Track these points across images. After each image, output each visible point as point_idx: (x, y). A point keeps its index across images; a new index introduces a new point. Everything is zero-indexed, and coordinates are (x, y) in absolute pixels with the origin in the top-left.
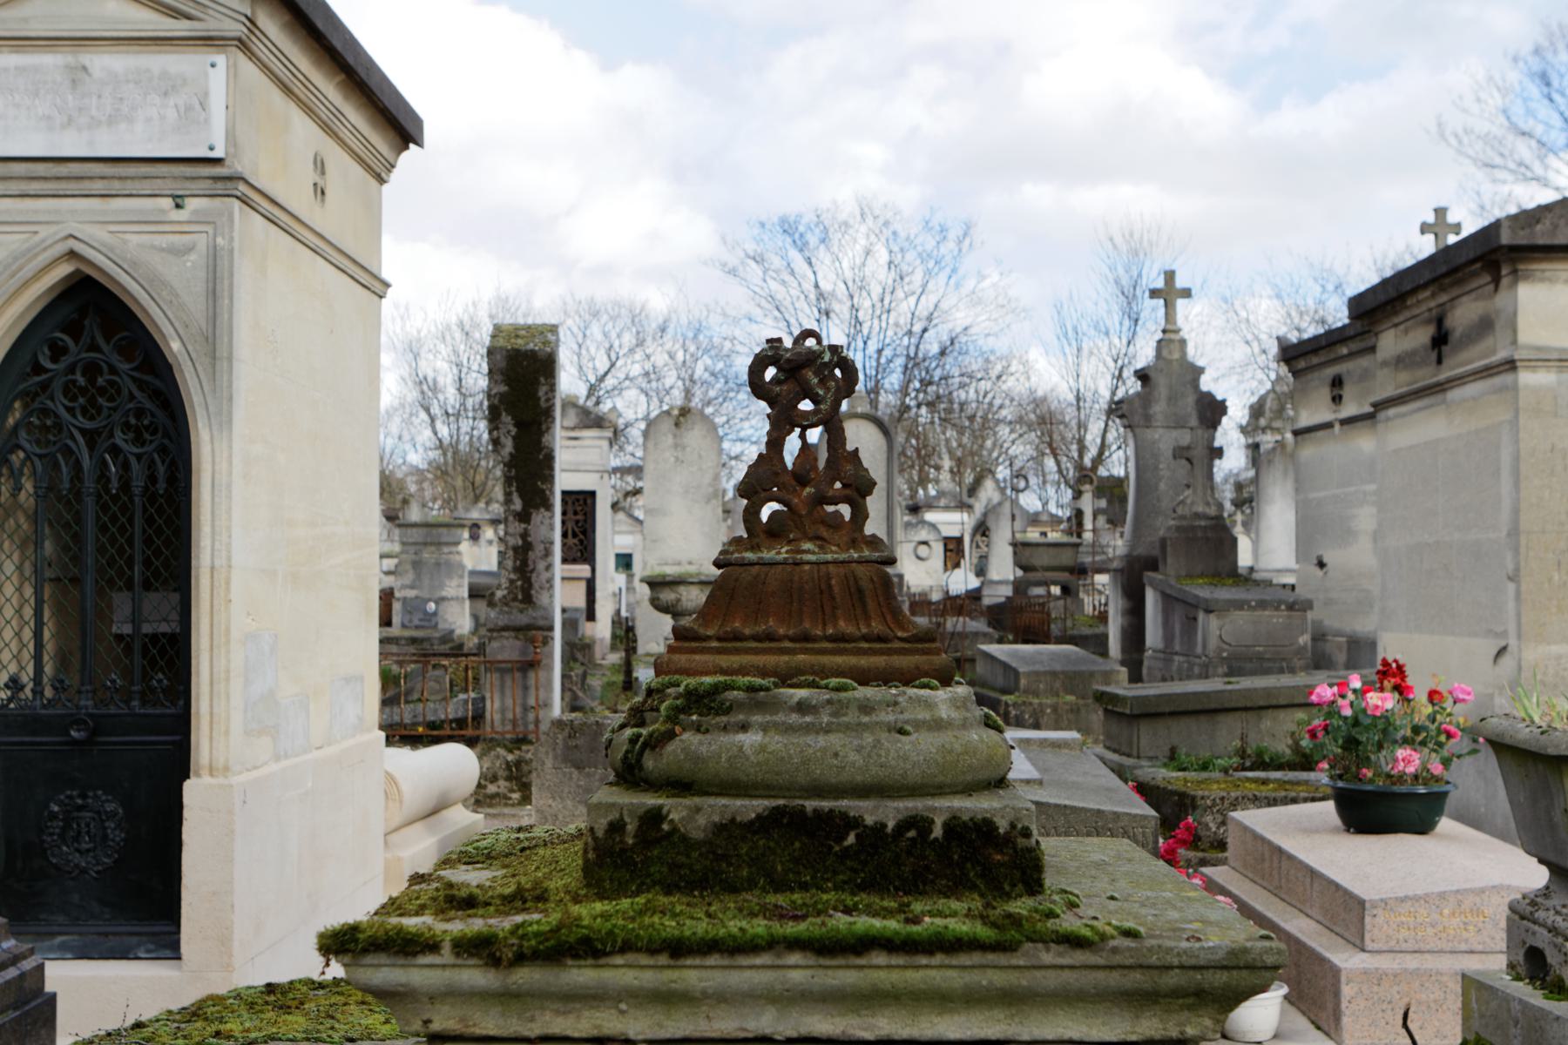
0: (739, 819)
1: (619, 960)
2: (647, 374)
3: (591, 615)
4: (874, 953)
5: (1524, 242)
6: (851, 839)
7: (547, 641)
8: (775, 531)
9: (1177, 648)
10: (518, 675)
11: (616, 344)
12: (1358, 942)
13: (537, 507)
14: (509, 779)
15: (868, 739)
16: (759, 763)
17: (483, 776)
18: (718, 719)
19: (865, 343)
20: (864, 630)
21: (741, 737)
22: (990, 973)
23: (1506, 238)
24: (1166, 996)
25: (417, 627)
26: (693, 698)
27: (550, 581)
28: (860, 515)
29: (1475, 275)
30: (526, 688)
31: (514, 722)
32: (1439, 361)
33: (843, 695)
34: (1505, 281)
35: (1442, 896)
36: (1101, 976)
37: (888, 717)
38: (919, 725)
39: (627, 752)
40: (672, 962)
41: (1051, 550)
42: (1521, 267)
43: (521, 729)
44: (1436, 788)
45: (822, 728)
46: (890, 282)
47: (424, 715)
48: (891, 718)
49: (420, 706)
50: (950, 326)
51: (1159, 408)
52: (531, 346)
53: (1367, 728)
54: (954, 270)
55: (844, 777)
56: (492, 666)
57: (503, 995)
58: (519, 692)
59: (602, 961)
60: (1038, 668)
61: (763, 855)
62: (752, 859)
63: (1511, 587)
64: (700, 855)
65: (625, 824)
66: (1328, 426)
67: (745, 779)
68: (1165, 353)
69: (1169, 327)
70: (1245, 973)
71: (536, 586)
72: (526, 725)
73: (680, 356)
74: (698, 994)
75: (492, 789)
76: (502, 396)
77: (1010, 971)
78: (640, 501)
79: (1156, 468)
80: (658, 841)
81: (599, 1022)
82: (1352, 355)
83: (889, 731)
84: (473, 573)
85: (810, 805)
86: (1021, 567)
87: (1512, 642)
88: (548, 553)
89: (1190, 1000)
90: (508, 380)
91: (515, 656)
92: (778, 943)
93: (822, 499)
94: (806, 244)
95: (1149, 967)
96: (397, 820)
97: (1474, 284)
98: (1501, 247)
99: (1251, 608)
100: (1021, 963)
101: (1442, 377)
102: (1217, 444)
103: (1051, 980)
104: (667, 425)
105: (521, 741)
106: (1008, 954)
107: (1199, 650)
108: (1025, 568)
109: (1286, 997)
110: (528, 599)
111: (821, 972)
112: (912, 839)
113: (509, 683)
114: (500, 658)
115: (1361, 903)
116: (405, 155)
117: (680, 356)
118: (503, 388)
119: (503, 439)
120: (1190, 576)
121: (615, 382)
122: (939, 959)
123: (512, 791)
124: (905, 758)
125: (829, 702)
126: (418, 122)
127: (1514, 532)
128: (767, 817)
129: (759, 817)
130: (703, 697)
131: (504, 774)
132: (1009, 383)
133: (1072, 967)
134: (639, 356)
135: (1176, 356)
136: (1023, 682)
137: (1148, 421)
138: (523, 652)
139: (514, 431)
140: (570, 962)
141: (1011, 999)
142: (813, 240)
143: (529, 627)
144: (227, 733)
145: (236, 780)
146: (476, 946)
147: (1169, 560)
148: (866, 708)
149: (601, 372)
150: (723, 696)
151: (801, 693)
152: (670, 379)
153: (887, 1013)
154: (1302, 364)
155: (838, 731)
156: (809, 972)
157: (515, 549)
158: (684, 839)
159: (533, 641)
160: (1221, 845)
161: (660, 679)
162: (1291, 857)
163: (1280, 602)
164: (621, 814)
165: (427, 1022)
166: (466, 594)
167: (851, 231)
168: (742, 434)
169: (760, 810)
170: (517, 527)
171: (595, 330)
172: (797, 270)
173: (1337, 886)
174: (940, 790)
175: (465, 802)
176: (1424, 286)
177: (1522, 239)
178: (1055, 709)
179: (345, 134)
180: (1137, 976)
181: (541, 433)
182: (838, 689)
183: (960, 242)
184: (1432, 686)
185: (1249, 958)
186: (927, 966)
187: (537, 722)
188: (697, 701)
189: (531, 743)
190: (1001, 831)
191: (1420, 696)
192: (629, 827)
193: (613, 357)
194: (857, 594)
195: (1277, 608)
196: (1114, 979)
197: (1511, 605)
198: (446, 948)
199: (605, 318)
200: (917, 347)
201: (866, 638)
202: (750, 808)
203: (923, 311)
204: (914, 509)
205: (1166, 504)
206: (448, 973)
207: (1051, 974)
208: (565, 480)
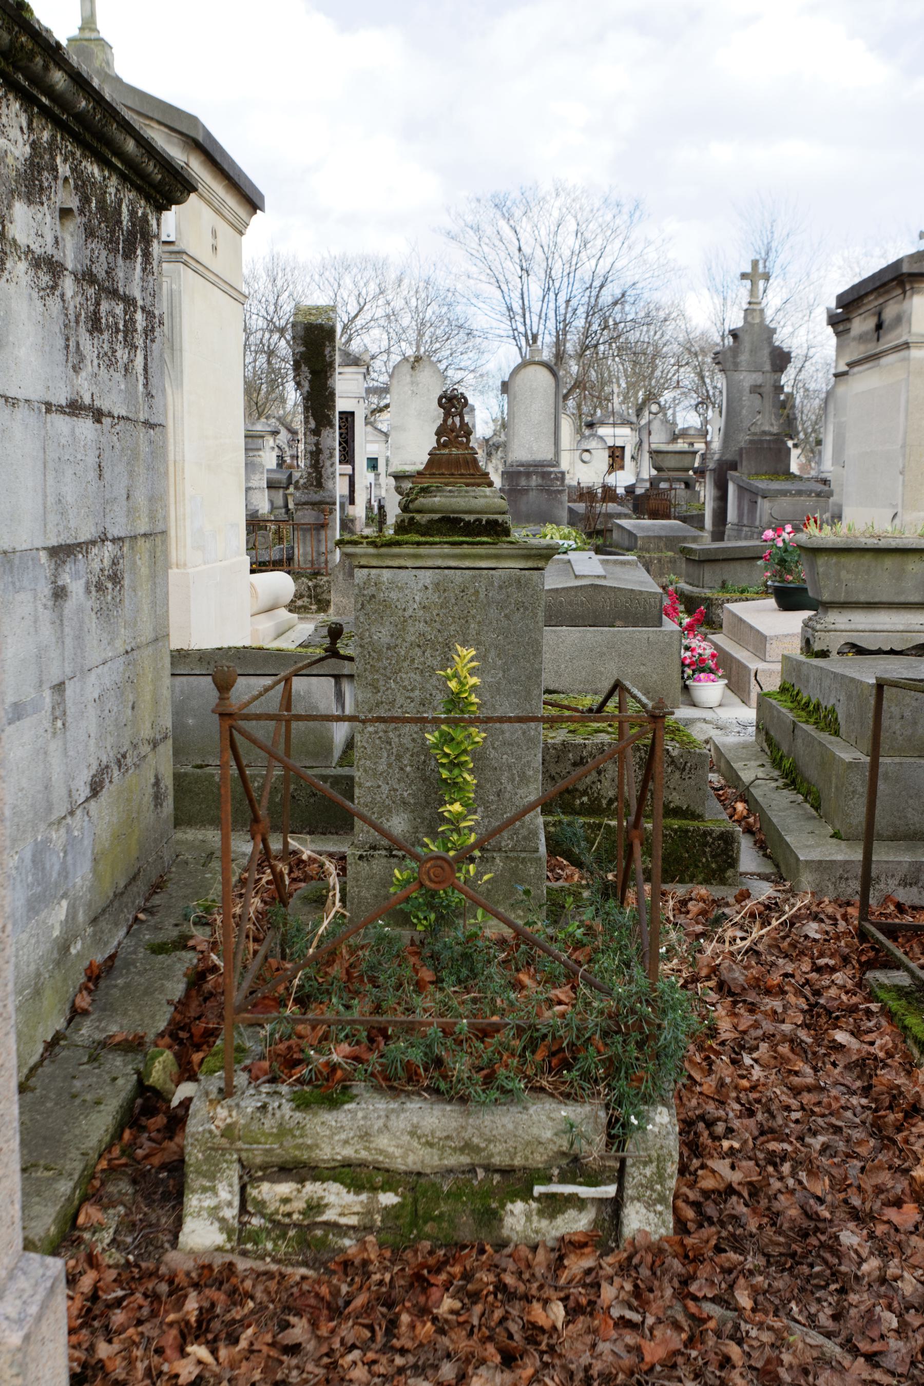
2: (388, 316)
3: (352, 502)
5: (916, 271)
7: (332, 511)
8: (445, 445)
9: (745, 522)
11: (364, 292)
13: (325, 426)
14: (310, 597)
19: (556, 295)
23: (905, 269)
27: (333, 473)
28: (468, 441)
29: (894, 288)
30: (319, 541)
31: (312, 562)
32: (878, 340)
34: (908, 293)
41: (677, 456)
42: (916, 285)
46: (577, 247)
50: (622, 281)
51: (744, 358)
52: (320, 321)
53: (791, 553)
54: (626, 238)
56: (296, 527)
58: (315, 543)
60: (651, 534)
63: (901, 477)
68: (749, 319)
69: (754, 300)
71: (325, 476)
73: (413, 302)
75: (299, 603)
78: (385, 416)
79: (741, 399)
86: (656, 468)
87: (900, 510)
88: (332, 456)
90: (305, 344)
91: (312, 521)
93: (458, 436)
94: (512, 215)
96: (255, 610)
97: (895, 294)
98: (903, 274)
99: (791, 495)
101: (882, 347)
103: (505, 552)
104: (407, 367)
105: (316, 574)
107: (757, 523)
108: (659, 469)
109: (726, 685)
110: (320, 485)
113: (308, 537)
115: (766, 637)
116: (255, 217)
118: (302, 349)
119: (303, 382)
120: (757, 474)
121: (364, 322)
126: (262, 197)
127: (904, 446)
132: (670, 327)
135: (757, 320)
136: (639, 543)
137: (736, 367)
138: (318, 518)
139: (310, 377)
141: (497, 557)
142: (518, 213)
143: (321, 503)
144: (185, 546)
145: (189, 571)
147: (744, 463)
148: (467, 492)
149: (353, 314)
152: (406, 320)
157: (311, 453)
159: (323, 511)
160: (721, 627)
162: (744, 622)
163: (811, 491)
167: (546, 206)
168: (462, 365)
170: (313, 439)
171: (347, 281)
172: (504, 236)
173: (758, 631)
174: (486, 513)
176: (871, 292)
177: (915, 269)
178: (659, 560)
179: (226, 213)
181: (327, 379)
183: (631, 216)
187: (326, 562)
193: (362, 302)
194: (467, 463)
195: (809, 496)
196: (520, 552)
197: (900, 488)
199: (355, 270)
200: (597, 297)
202: (437, 516)
203: (601, 271)
204: (591, 425)
205: (746, 424)
208: (342, 405)
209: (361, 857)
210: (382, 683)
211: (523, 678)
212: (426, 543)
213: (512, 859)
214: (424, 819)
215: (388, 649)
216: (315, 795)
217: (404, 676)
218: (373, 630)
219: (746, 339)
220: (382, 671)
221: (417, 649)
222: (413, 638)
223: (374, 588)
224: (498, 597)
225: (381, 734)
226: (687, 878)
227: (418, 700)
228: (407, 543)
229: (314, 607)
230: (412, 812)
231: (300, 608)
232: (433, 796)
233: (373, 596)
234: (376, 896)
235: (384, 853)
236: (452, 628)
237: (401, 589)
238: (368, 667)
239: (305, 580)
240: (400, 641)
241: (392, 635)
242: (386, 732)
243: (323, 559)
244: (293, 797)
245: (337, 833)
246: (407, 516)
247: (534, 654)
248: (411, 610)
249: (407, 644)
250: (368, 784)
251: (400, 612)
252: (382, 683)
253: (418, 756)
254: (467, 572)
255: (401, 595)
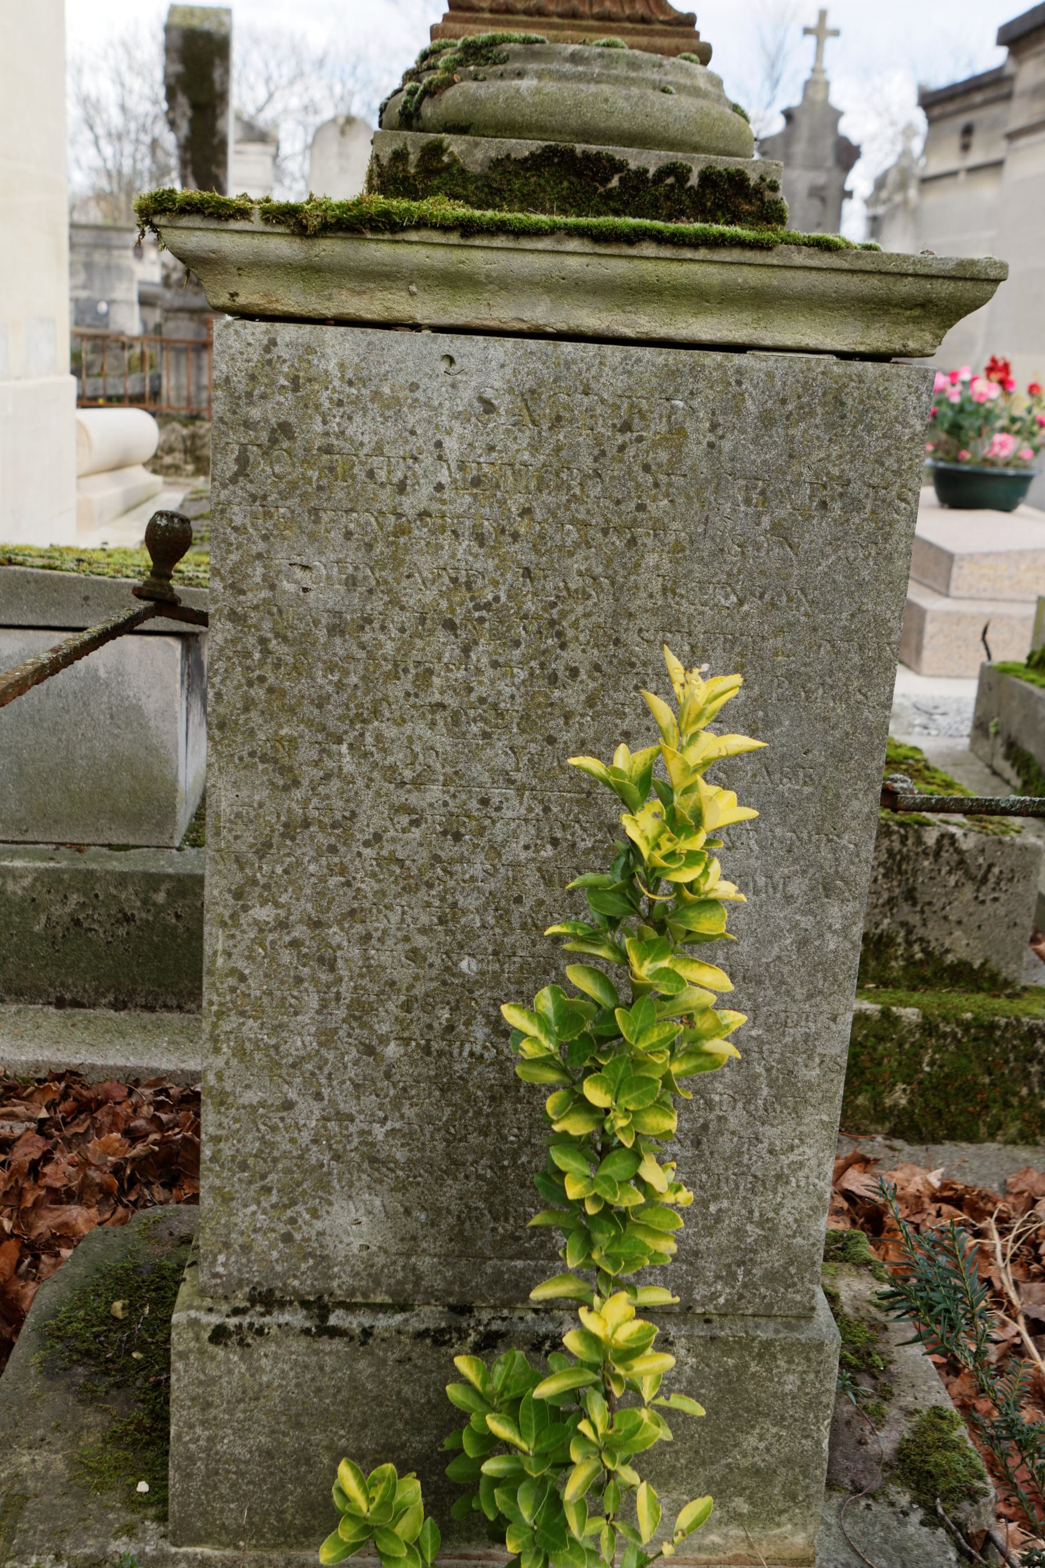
0: (513, 156)
1: (413, 236)
4: (645, 245)
6: (615, 182)
10: (192, 355)
12: (943, 590)
14: (186, 451)
15: (635, 91)
16: (534, 104)
17: (160, 448)
18: (495, 68)
20: (628, 11)
21: (516, 82)
22: (746, 270)
24: (896, 306)
25: (89, 326)
26: (471, 51)
30: (199, 368)
33: (613, 50)
35: (1021, 553)
36: (843, 279)
37: (655, 76)
38: (681, 88)
39: (406, 102)
40: (462, 242)
43: (194, 406)
44: (1023, 472)
45: (593, 79)
47: (105, 389)
48: (656, 77)
49: (100, 381)
51: (799, 148)
53: (971, 414)
55: (613, 122)
57: (304, 269)
58: (193, 372)
59: (399, 237)
61: (534, 191)
62: (523, 195)
64: (477, 188)
65: (408, 154)
66: (953, 174)
67: (520, 119)
68: (810, 92)
70: (969, 285)
72: (199, 403)
73: (338, 89)
74: (482, 278)
75: (168, 460)
76: (179, 77)
77: (764, 270)
80: (438, 172)
81: (389, 304)
82: (986, 103)
83: (654, 89)
84: (141, 283)
85: (579, 148)
89: (917, 312)
92: (559, 229)
95: (887, 273)
96: (86, 467)
100: (775, 262)
102: (848, 187)
103: (799, 281)
104: (333, 133)
105: (194, 418)
106: (764, 253)
111: (595, 260)
112: (672, 186)
114: (175, 337)
115: (950, 557)
117: (338, 89)
122: (702, 253)
123: (186, 462)
124: (669, 112)
125: (601, 55)
128: (539, 155)
129: (532, 154)
130: (481, 47)
131: (181, 446)
133: (819, 269)
134: (298, 87)
138: (198, 333)
139: (189, 113)
140: (369, 236)
146: (284, 214)
148: (633, 65)
150: (500, 47)
151: (572, 48)
153: (649, 310)
154: (937, 111)
155: (608, 82)
156: (584, 260)
158: (463, 171)
161: (436, 41)
164: (405, 144)
165: (233, 295)
166: (135, 298)
169: (533, 149)
175: (145, 465)
180: (874, 281)
182: (608, 45)
184: (1031, 381)
185: (975, 270)
186: (691, 260)
188: (474, 54)
189: (203, 419)
190: (752, 183)
191: (1020, 390)
192: (412, 157)
198: (256, 216)
201: (630, 19)
202: (524, 147)
206: (257, 242)
207: (800, 274)
209: (219, 1335)
210: (307, 753)
211: (818, 755)
212: (500, 228)
213: (727, 1347)
214: (437, 1212)
215: (336, 630)
216: (128, 919)
217: (390, 732)
218: (280, 559)
219: (804, 124)
220: (309, 710)
221: (442, 636)
222: (429, 596)
223: (287, 400)
224: (754, 458)
225: (300, 931)
226: (983, 1130)
227: (436, 819)
228: (422, 223)
229: (190, 468)
230: (401, 1187)
231: (169, 467)
232: (474, 1139)
233: (285, 429)
234: (269, 1454)
235: (296, 1318)
236: (577, 564)
237: (392, 407)
238: (259, 693)
239: (176, 425)
240: (377, 604)
241: (352, 583)
242: (317, 924)
243: (204, 395)
244: (77, 923)
245: (180, 1008)
246: (413, 142)
247: (864, 671)
248: (426, 490)
249: (406, 618)
250: (251, 1097)
251: (385, 494)
252: (307, 753)
253: (428, 1007)
254: (647, 353)
255: (390, 432)
